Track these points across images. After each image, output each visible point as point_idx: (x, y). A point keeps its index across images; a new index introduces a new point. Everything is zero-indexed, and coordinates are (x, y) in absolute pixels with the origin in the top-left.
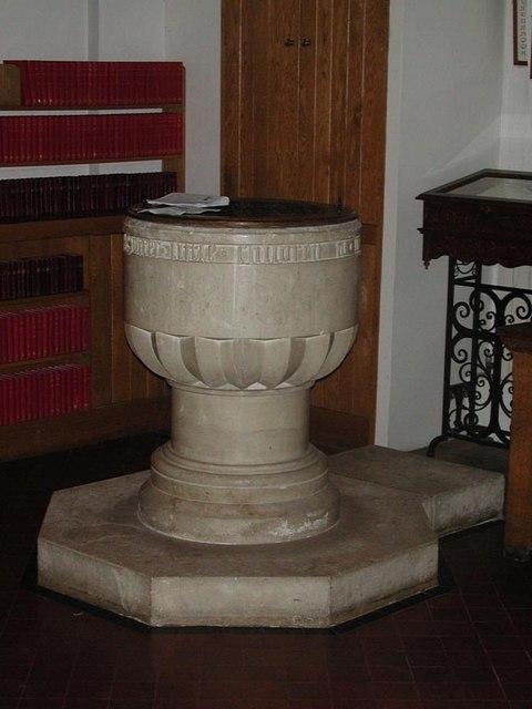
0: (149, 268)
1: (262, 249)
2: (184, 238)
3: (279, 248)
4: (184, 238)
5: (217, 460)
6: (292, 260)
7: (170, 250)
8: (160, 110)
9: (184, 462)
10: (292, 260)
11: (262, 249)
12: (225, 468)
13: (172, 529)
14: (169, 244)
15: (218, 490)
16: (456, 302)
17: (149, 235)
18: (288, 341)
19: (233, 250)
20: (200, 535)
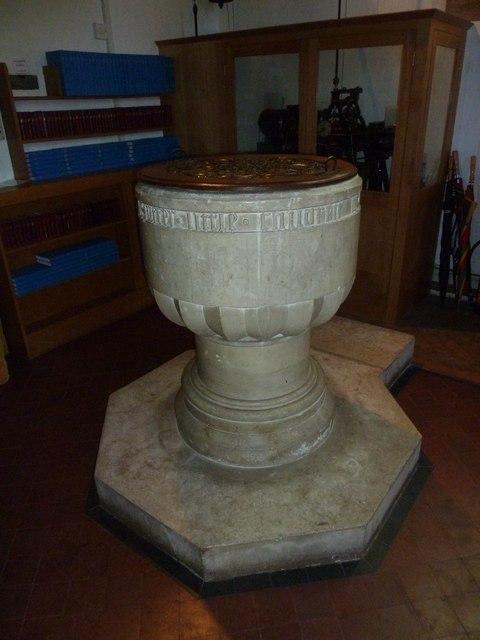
0: (165, 238)
1: (287, 214)
2: (201, 207)
3: (303, 211)
4: (201, 207)
5: (241, 397)
6: (315, 224)
7: (187, 219)
8: (160, 134)
9: (212, 396)
10: (315, 224)
11: (287, 214)
12: (247, 404)
13: (207, 454)
14: (184, 213)
15: (246, 421)
16: (339, 87)
17: (162, 204)
18: (312, 301)
19: (255, 218)
20: (233, 462)
